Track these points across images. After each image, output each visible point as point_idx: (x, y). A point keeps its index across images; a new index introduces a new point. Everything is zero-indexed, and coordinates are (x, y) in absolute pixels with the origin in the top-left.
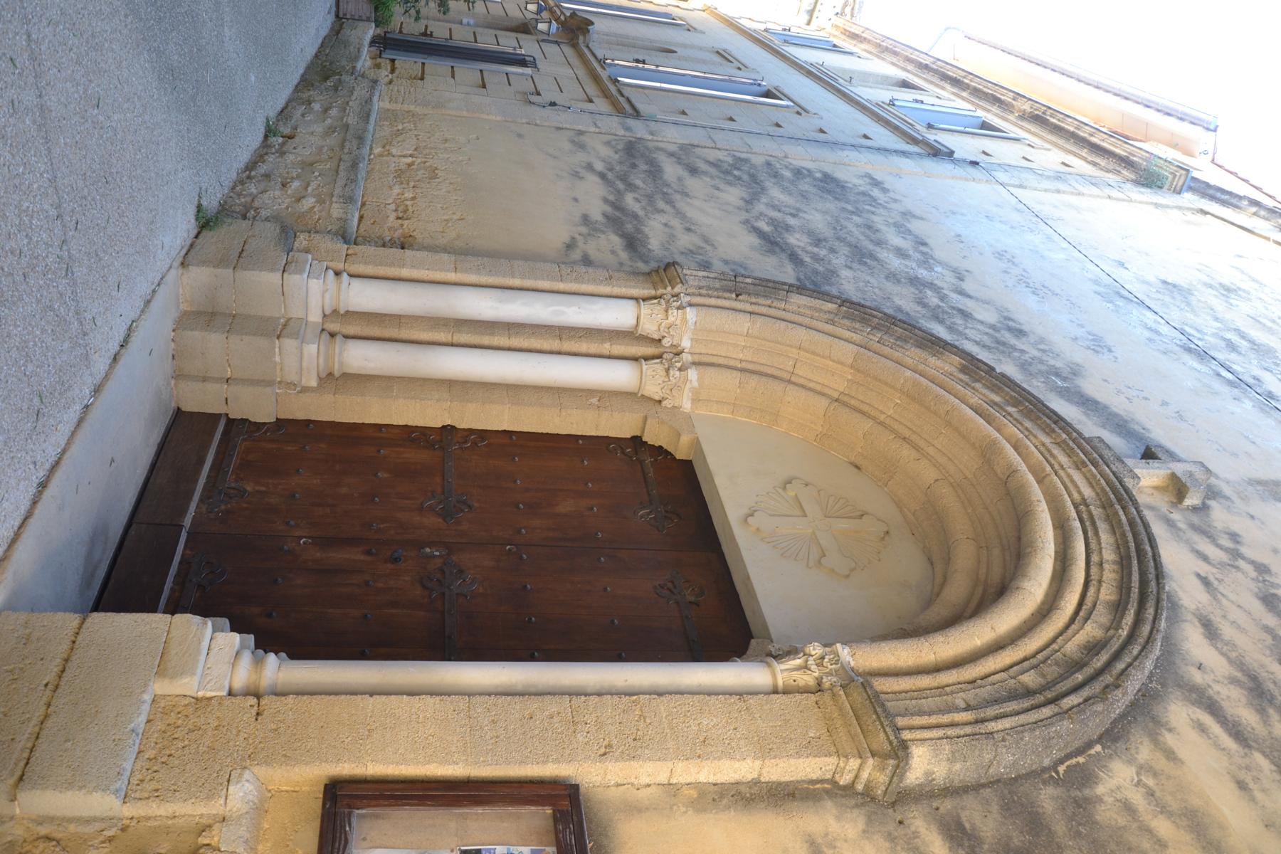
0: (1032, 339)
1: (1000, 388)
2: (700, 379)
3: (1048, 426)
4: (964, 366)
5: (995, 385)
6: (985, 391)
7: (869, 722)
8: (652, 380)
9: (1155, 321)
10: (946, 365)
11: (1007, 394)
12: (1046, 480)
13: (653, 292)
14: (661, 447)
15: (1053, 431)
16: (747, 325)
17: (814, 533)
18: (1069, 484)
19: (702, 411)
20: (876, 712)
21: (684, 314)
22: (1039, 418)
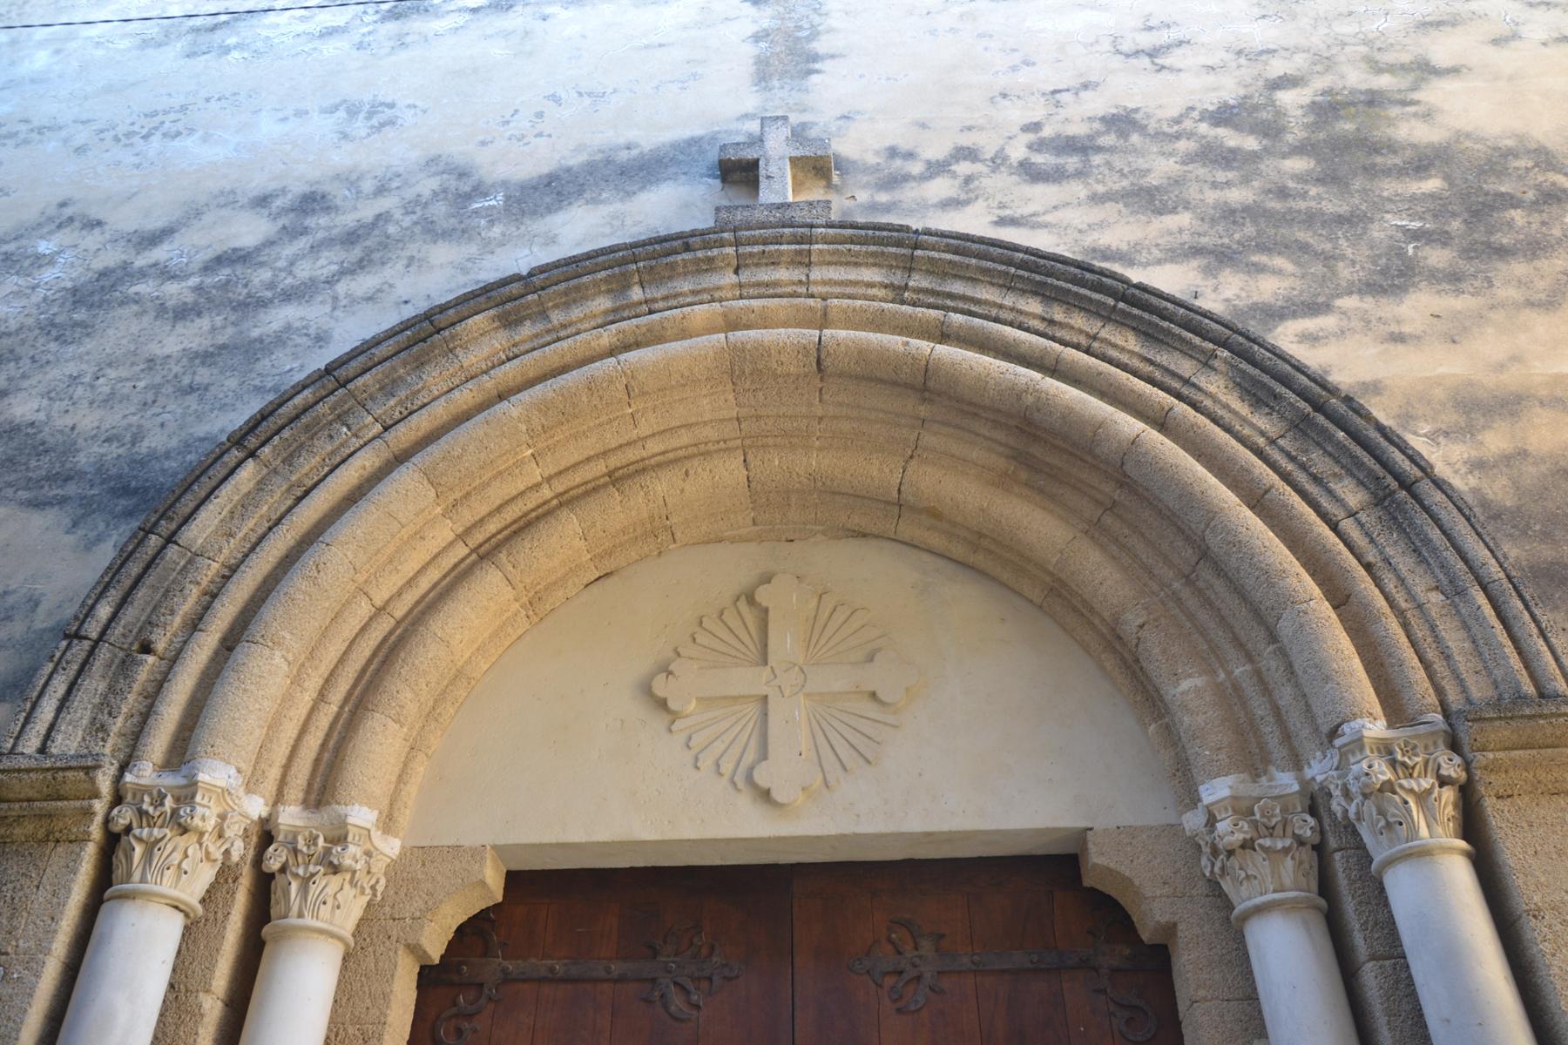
0: (339, 193)
1: (577, 288)
2: (369, 802)
3: (697, 261)
4: (499, 317)
5: (566, 293)
6: (576, 313)
7: (1549, 731)
8: (324, 919)
9: (303, 19)
10: (482, 341)
11: (596, 284)
12: (833, 314)
13: (90, 852)
14: (460, 930)
15: (710, 260)
16: (278, 658)
17: (807, 695)
18: (848, 290)
19: (405, 818)
20: (1530, 717)
21: (211, 789)
22: (672, 266)
